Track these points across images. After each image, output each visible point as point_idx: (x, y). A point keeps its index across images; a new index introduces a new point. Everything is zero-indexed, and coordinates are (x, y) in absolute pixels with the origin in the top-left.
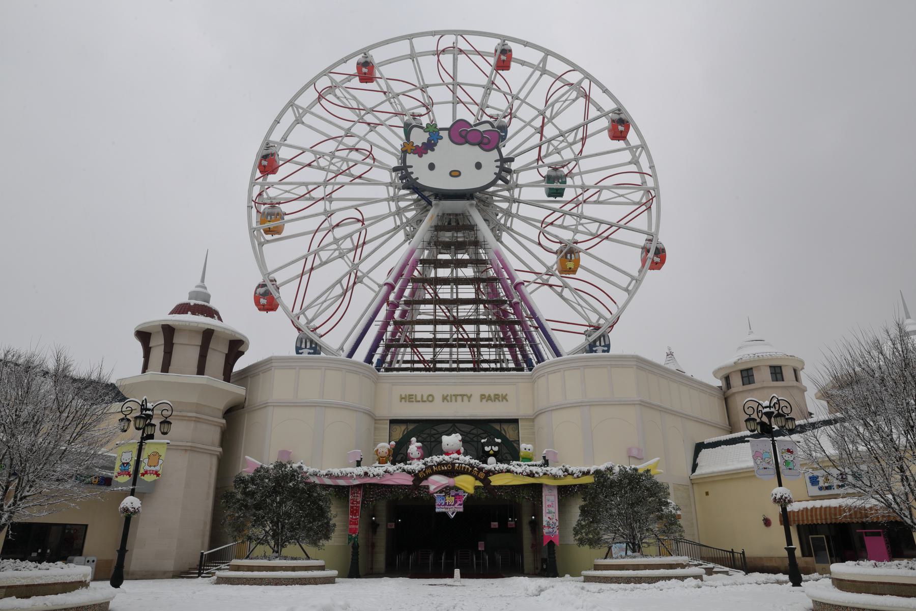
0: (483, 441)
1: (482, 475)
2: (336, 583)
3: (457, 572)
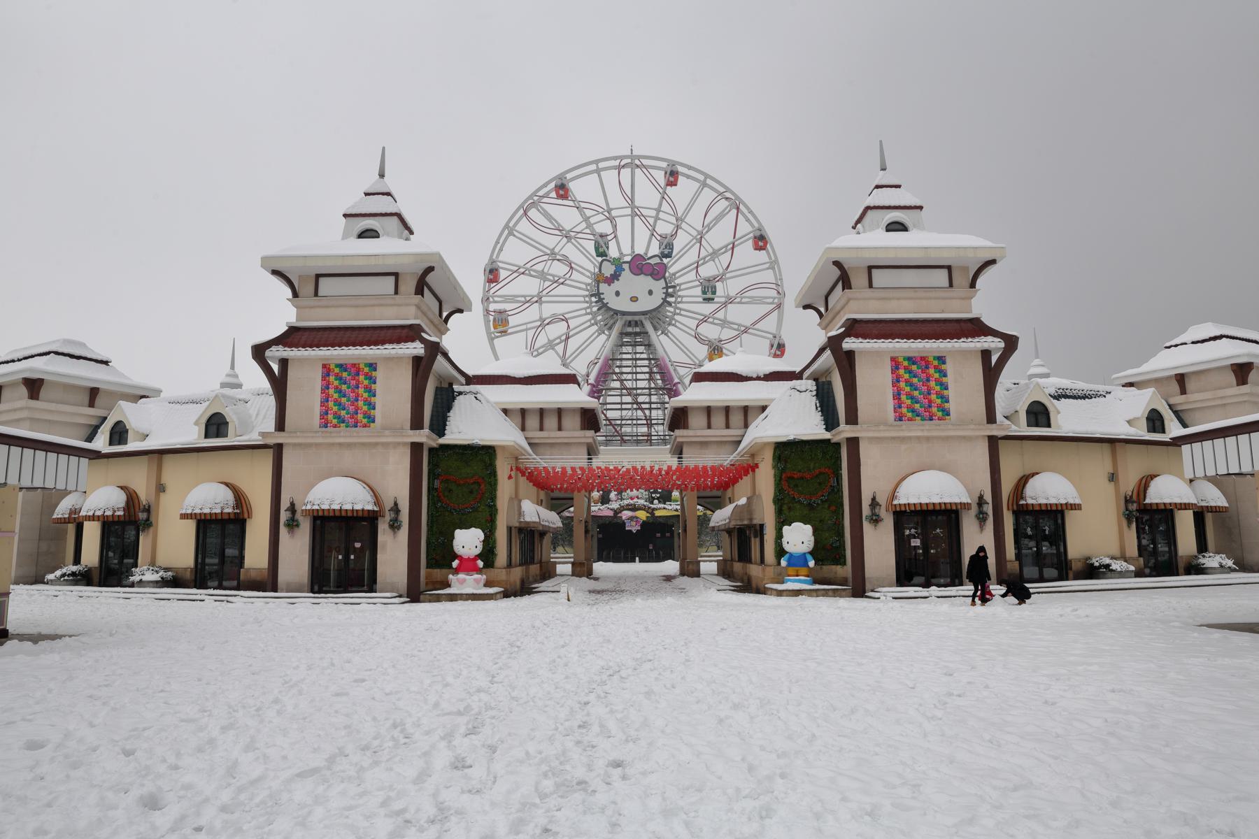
1: (650, 511)
3: (637, 559)
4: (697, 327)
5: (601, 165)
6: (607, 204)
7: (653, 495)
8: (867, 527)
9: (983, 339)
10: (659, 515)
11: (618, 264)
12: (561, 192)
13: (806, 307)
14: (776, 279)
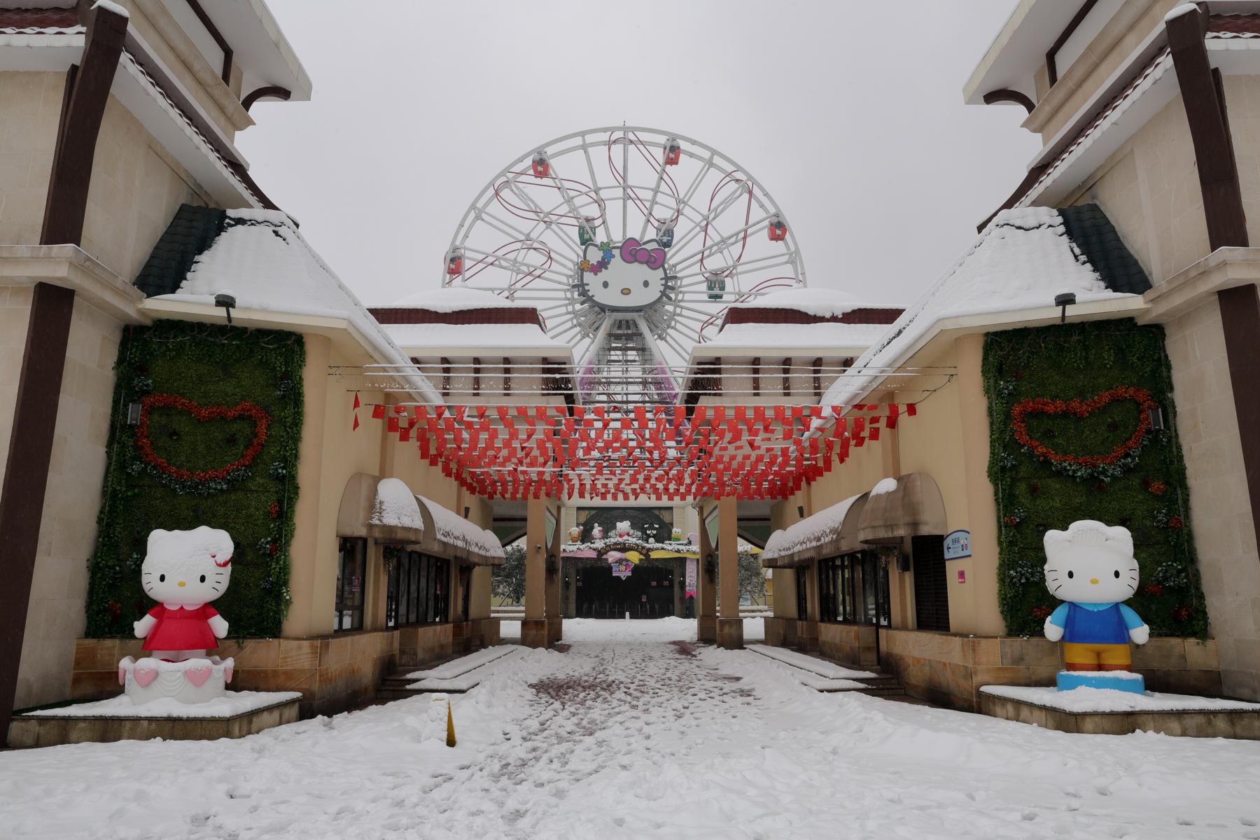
0: (645, 526)
1: (644, 551)
3: (627, 614)
4: (702, 330)
7: (648, 532)
10: (655, 557)
11: (607, 249)
12: (540, 169)
13: (992, 97)
14: (796, 273)
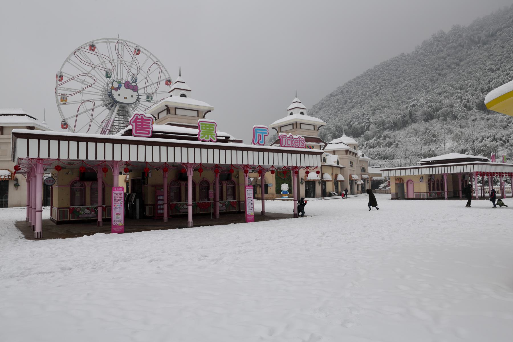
2: (306, 216)
5: (151, 56)
6: (142, 66)
8: (300, 184)
9: (321, 143)
